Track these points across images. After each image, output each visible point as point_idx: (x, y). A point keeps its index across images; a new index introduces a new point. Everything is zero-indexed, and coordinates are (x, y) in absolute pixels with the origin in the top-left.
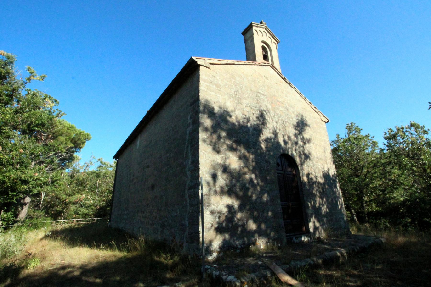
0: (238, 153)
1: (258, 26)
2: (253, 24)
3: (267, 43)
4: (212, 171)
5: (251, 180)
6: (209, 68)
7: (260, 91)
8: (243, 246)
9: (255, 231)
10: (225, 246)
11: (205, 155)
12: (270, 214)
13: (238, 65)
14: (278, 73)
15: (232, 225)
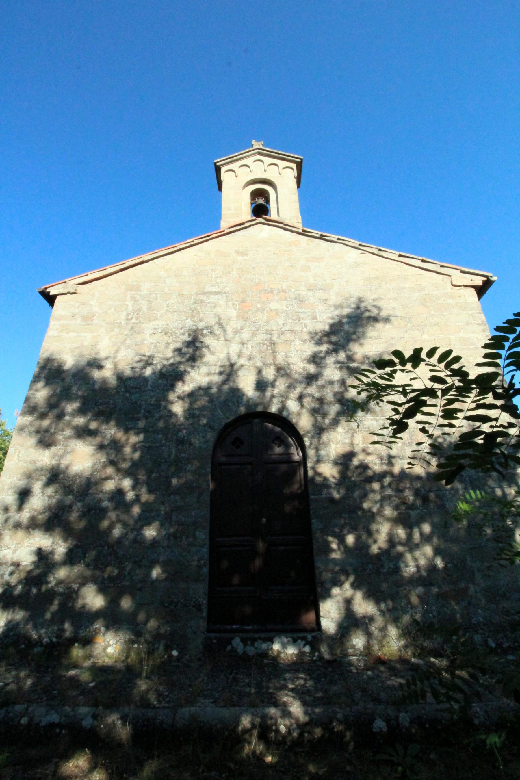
0: (98, 439)
1: (235, 158)
2: (218, 164)
3: (265, 179)
4: (22, 483)
5: (120, 492)
6: (74, 293)
7: (208, 289)
8: (54, 640)
9: (98, 614)
10: (11, 634)
11: (19, 452)
12: (156, 573)
13: (156, 260)
14: (285, 229)
15: (39, 590)
